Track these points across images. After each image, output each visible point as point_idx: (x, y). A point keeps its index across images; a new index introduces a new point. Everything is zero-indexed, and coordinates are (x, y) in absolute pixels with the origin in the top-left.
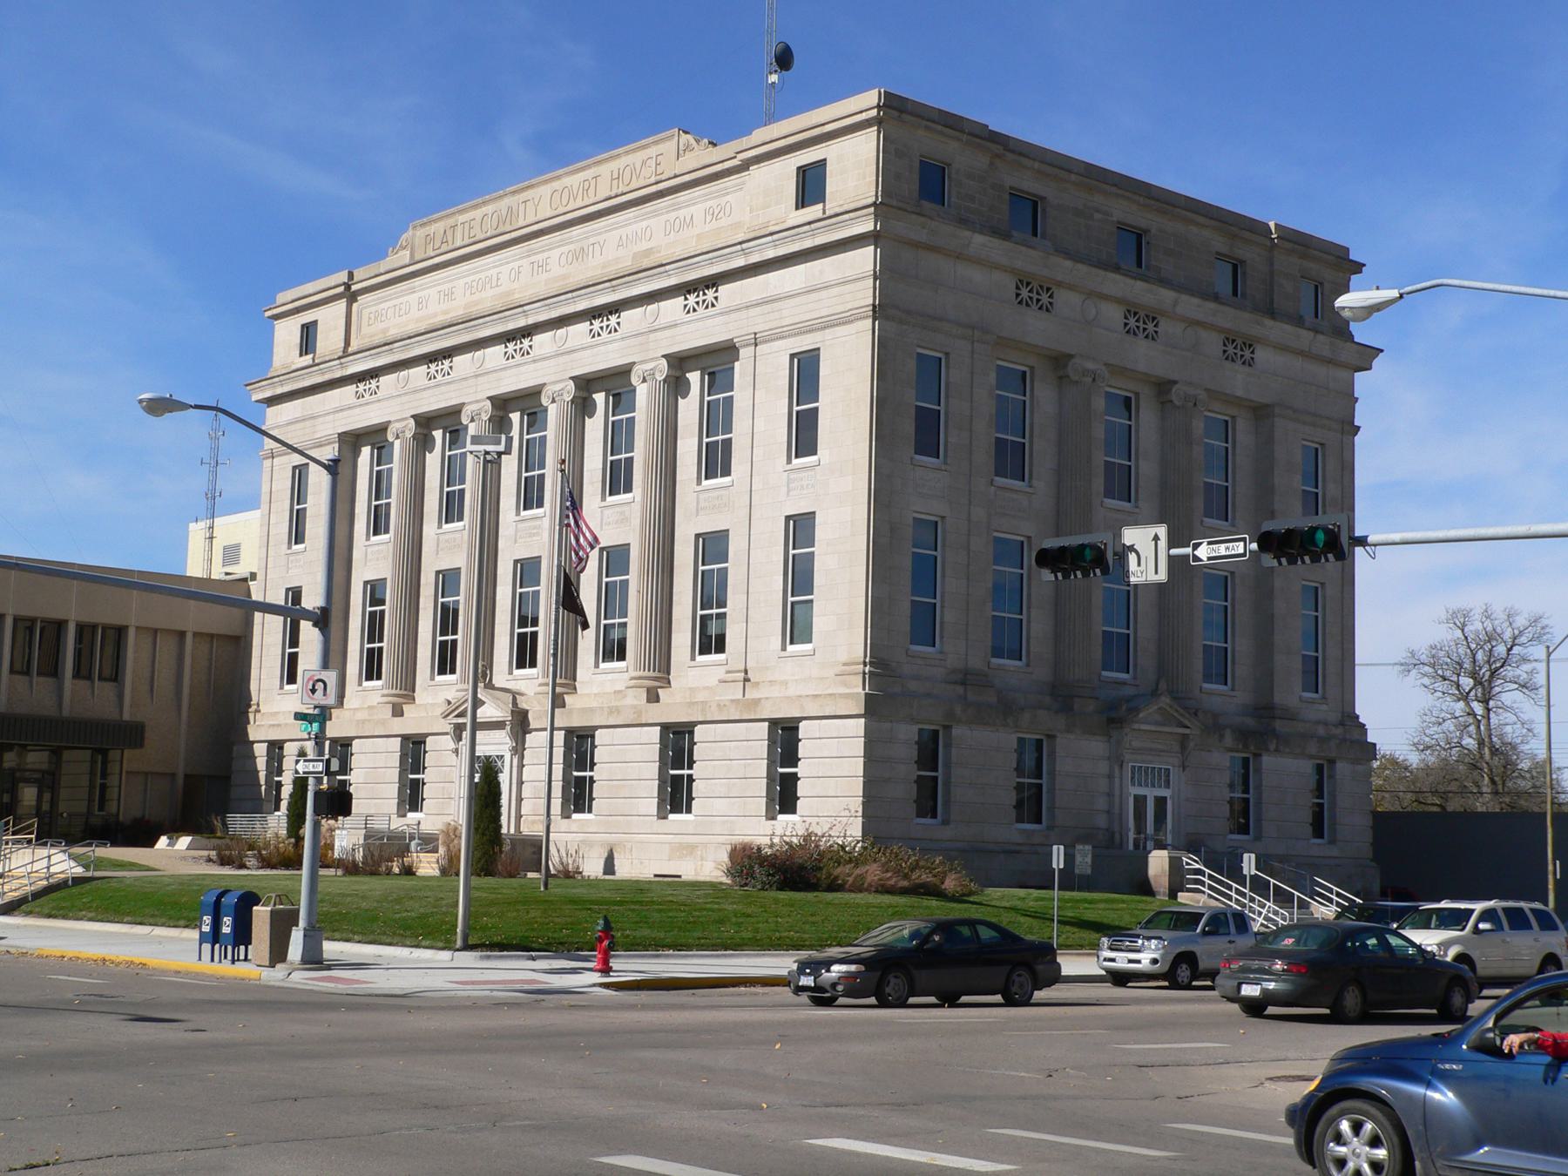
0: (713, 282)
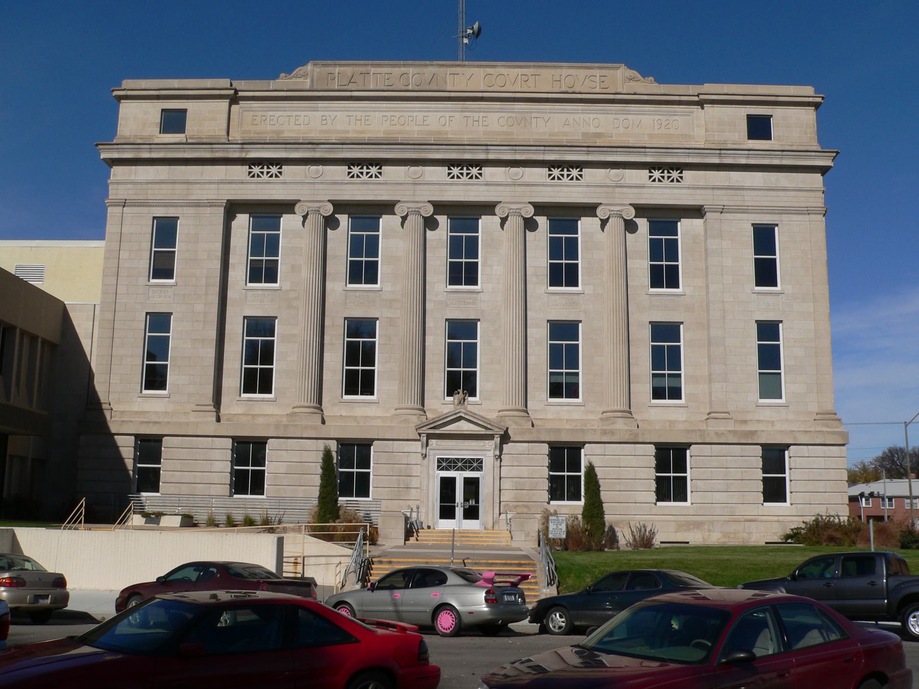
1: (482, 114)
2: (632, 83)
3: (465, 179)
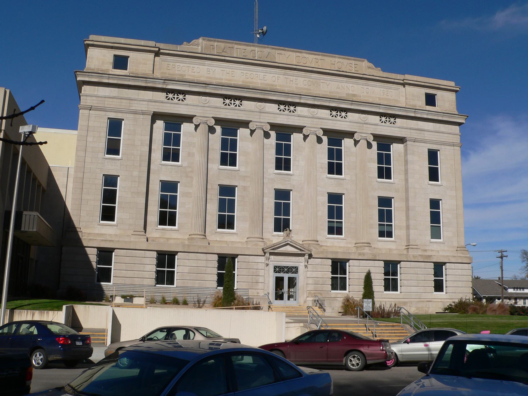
0: (395, 116)
1: (295, 78)
2: (370, 70)
3: (287, 112)
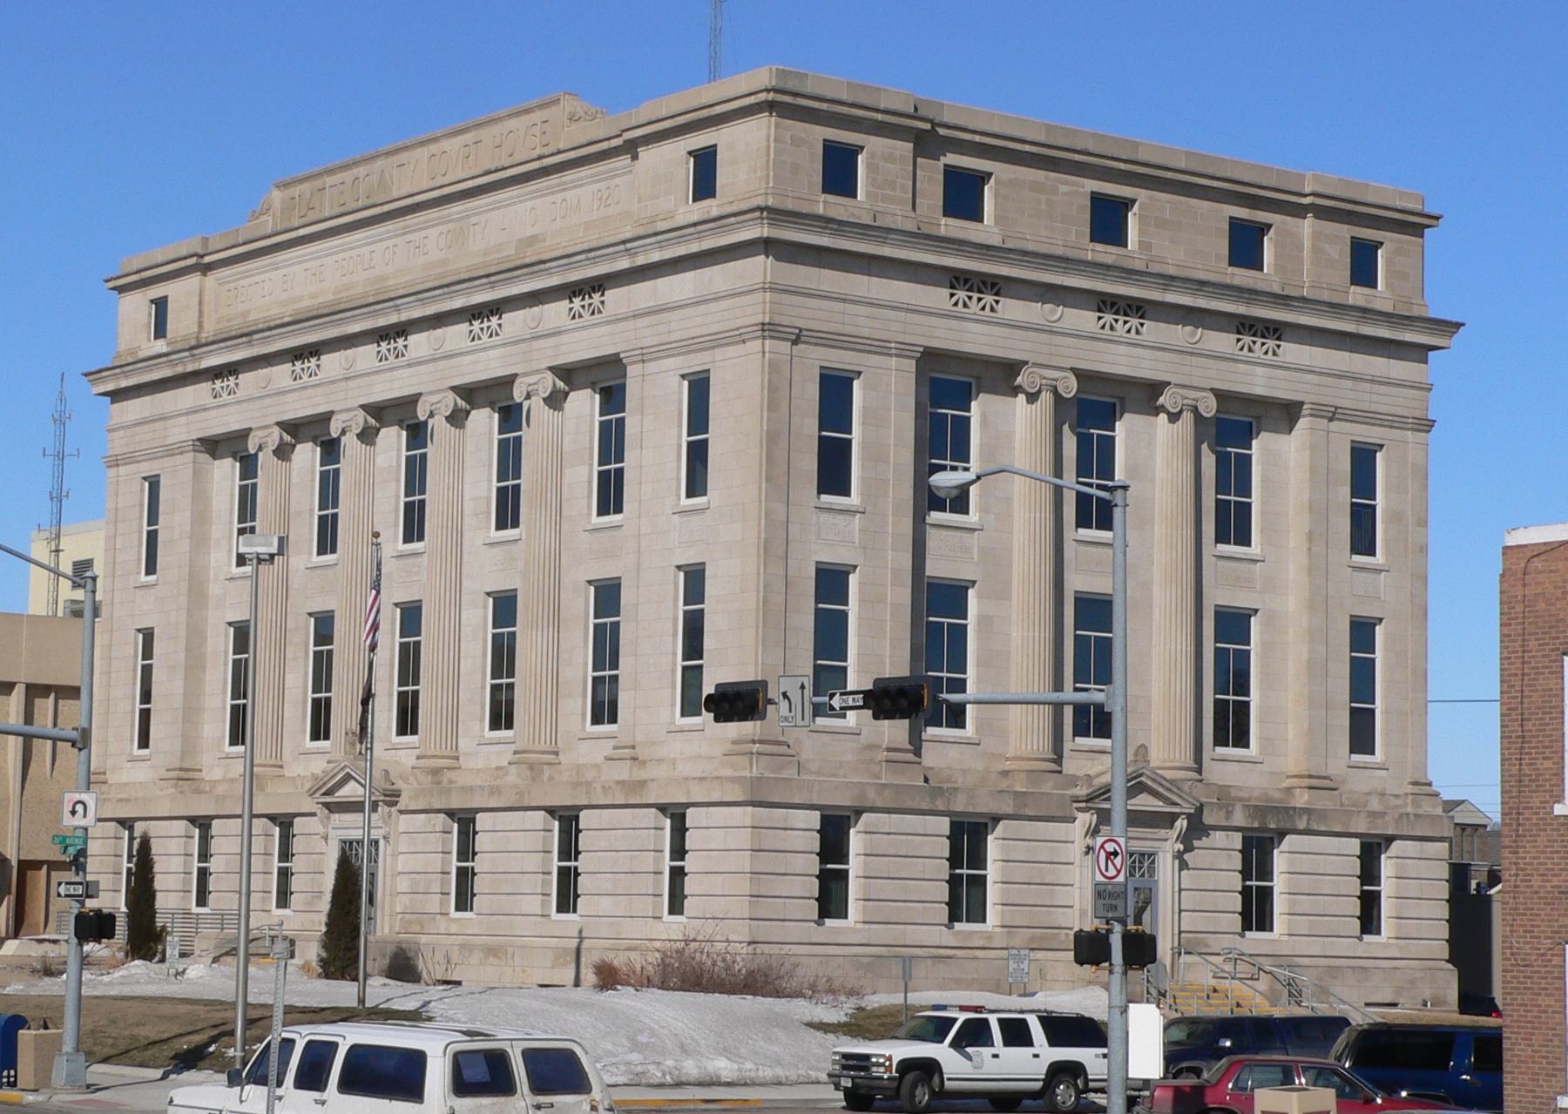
0: (598, 285)
